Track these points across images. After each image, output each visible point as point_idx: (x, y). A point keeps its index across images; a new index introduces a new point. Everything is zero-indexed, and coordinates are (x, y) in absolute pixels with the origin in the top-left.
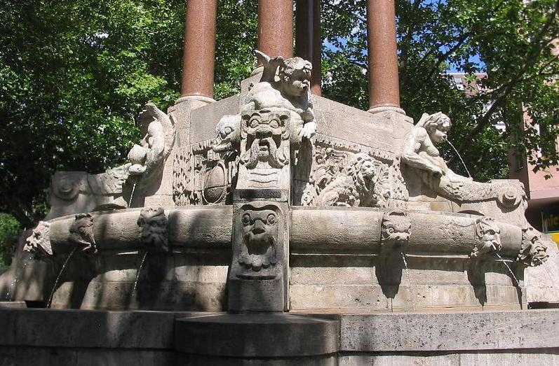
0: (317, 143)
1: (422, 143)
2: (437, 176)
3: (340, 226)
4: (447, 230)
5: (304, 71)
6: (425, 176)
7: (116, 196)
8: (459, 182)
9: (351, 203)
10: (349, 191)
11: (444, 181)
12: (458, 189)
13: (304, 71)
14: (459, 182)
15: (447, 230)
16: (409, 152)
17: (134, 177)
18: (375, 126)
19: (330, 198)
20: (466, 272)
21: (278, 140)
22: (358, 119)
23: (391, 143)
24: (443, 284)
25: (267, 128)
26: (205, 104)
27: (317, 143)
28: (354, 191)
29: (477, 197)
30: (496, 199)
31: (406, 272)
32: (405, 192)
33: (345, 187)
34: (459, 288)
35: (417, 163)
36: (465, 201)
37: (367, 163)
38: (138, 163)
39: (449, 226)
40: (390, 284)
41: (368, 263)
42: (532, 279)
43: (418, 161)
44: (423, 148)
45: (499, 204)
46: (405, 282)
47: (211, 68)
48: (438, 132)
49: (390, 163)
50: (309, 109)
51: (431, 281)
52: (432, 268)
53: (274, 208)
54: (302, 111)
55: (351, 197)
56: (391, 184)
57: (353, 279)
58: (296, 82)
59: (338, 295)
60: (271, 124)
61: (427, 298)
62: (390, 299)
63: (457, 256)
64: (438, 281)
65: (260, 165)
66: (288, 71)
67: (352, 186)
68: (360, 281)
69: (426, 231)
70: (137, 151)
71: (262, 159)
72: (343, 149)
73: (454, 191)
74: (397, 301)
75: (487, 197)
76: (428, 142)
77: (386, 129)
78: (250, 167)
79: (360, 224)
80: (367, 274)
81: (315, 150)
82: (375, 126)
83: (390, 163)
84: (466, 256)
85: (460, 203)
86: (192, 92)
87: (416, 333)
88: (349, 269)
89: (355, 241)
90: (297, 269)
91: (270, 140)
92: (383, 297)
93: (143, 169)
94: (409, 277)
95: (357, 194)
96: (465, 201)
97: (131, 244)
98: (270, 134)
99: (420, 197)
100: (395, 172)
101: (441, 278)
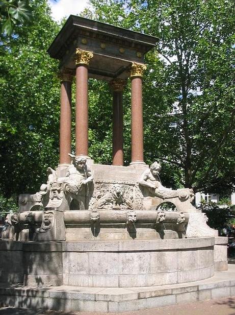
2: (154, 189)
3: (78, 216)
7: (39, 202)
9: (112, 203)
11: (157, 191)
16: (141, 180)
17: (43, 196)
18: (126, 172)
21: (59, 191)
22: (117, 171)
25: (55, 188)
26: (66, 167)
27: (96, 183)
32: (142, 196)
36: (166, 198)
37: (117, 188)
38: (43, 191)
40: (96, 233)
41: (87, 227)
44: (148, 178)
47: (141, 107)
48: (154, 172)
49: (134, 185)
50: (89, 172)
53: (52, 213)
56: (135, 194)
57: (84, 231)
58: (79, 165)
59: (79, 236)
65: (54, 198)
66: (76, 162)
70: (43, 186)
71: (55, 197)
72: (109, 183)
74: (98, 238)
76: (151, 176)
78: (52, 200)
80: (88, 230)
81: (96, 186)
82: (126, 172)
83: (134, 185)
85: (164, 199)
86: (63, 163)
87: (78, 247)
88: (83, 228)
90: (70, 230)
91: (56, 191)
93: (45, 193)
94: (102, 230)
96: (166, 198)
97: (27, 222)
98: (56, 190)
100: (137, 189)
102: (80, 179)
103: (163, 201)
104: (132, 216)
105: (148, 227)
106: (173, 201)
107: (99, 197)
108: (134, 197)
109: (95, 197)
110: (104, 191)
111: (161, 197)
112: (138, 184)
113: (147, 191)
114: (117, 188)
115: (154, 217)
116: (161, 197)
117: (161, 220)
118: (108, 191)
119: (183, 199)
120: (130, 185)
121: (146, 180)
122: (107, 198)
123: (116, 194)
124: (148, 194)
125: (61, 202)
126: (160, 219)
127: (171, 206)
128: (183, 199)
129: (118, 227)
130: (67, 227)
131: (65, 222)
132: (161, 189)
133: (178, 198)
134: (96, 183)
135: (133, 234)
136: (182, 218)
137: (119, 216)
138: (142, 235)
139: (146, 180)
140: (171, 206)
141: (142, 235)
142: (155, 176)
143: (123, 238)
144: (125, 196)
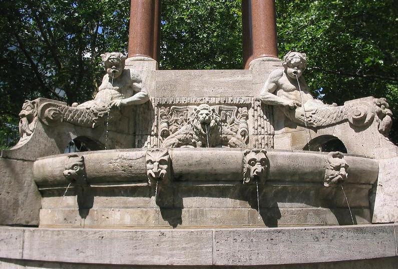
0: (159, 105)
1: (276, 83)
2: (291, 109)
4: (116, 164)
5: (110, 61)
6: (284, 110)
8: (312, 110)
9: (195, 145)
10: (190, 136)
11: (299, 111)
12: (311, 117)
13: (110, 61)
14: (312, 110)
15: (116, 164)
16: (264, 93)
18: (228, 79)
19: (168, 144)
20: (154, 198)
23: (250, 89)
24: (127, 208)
28: (194, 135)
29: (329, 121)
30: (346, 120)
31: (96, 199)
32: (267, 125)
33: (186, 134)
34: (142, 211)
35: (269, 101)
39: (118, 161)
42: (388, 197)
43: (269, 99)
45: (351, 125)
46: (95, 207)
49: (248, 106)
50: (135, 84)
51: (115, 205)
52: (211, 195)
54: (118, 88)
55: (193, 141)
60: (27, 108)
61: (110, 218)
62: (83, 219)
63: (116, 186)
64: (122, 206)
67: (192, 132)
68: (68, 206)
69: (98, 166)
72: (188, 104)
73: (308, 119)
74: (87, 221)
75: (339, 120)
76: (285, 81)
77: (242, 79)
79: (58, 166)
82: (228, 79)
83: (248, 106)
84: (145, 184)
89: (59, 178)
90: (47, 201)
92: (79, 217)
95: (197, 138)
99: (284, 130)
101: (125, 203)
102: (109, 97)
103: (314, 135)
104: (152, 163)
105: (222, 193)
106: (338, 132)
107: (165, 134)
108: (251, 131)
109: (156, 135)
110: (176, 121)
111: (310, 126)
112: (259, 103)
113: (279, 115)
114: (202, 112)
115: (234, 166)
116: (310, 126)
117: (252, 174)
118: (186, 120)
119: (360, 124)
120: (240, 106)
121: (275, 93)
122: (182, 136)
123: (199, 127)
124: (282, 123)
125: (30, 138)
126: (249, 170)
127: (334, 145)
128: (360, 124)
129: (133, 192)
130: (43, 194)
131: (39, 184)
132: (310, 106)
133: (347, 124)
134: (159, 105)
135: (172, 213)
136: (338, 168)
137: (126, 163)
138: (199, 214)
139: (275, 93)
140: (334, 145)
141: (199, 214)
142: (293, 81)
143: (143, 221)
144: (226, 129)
